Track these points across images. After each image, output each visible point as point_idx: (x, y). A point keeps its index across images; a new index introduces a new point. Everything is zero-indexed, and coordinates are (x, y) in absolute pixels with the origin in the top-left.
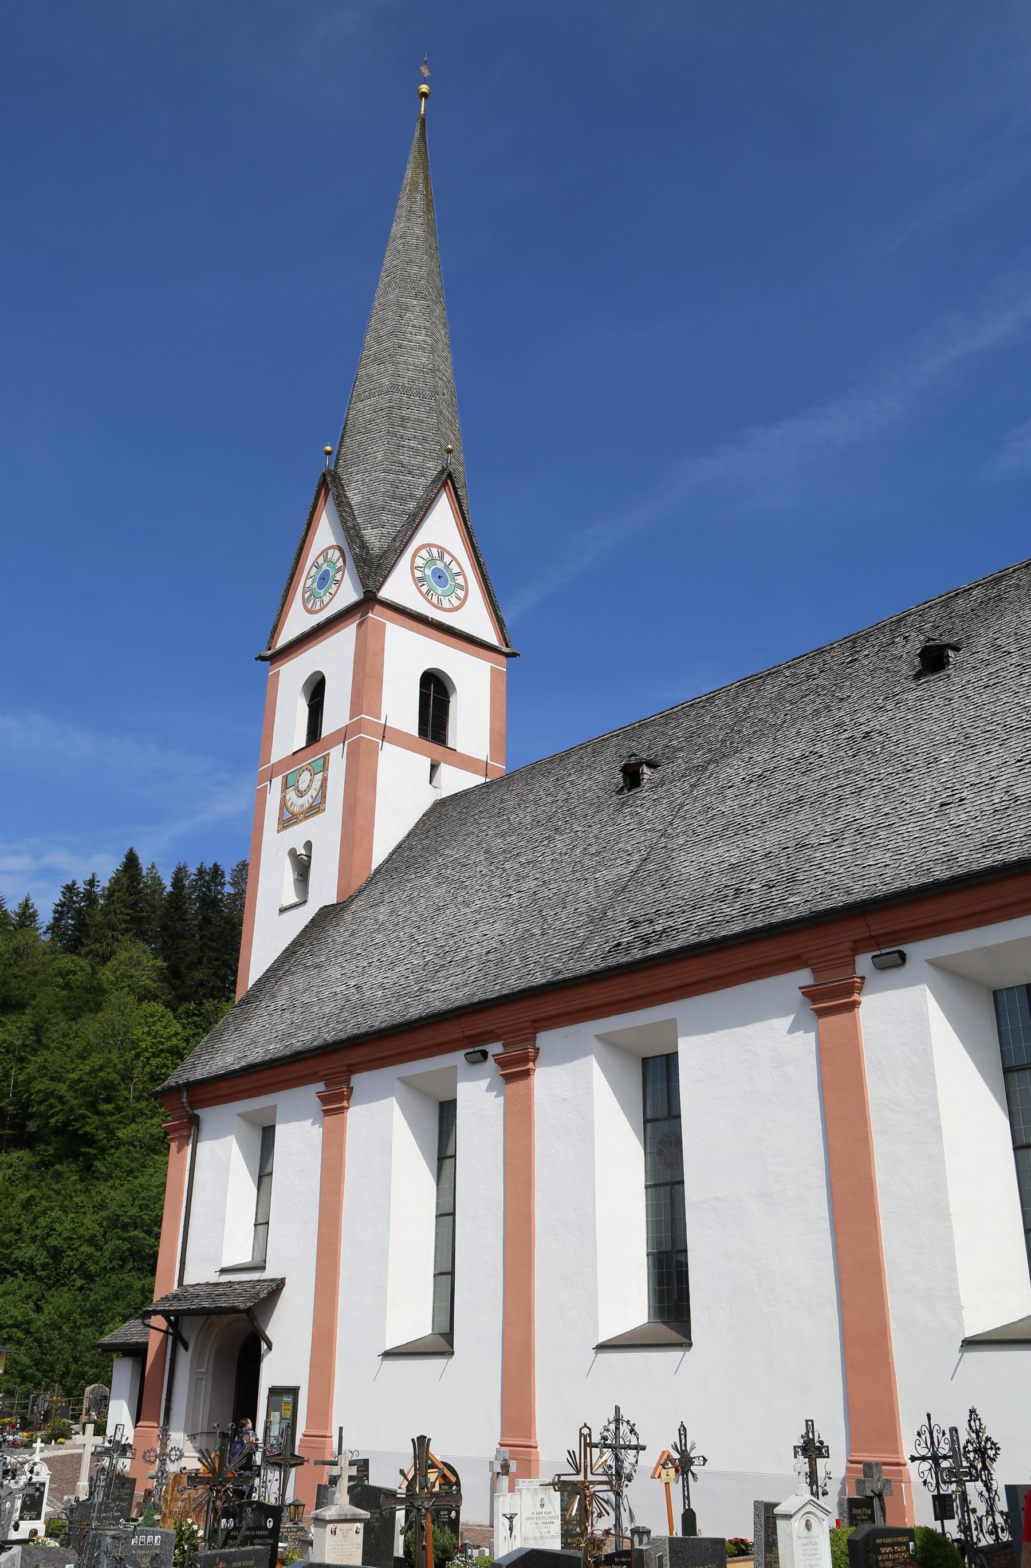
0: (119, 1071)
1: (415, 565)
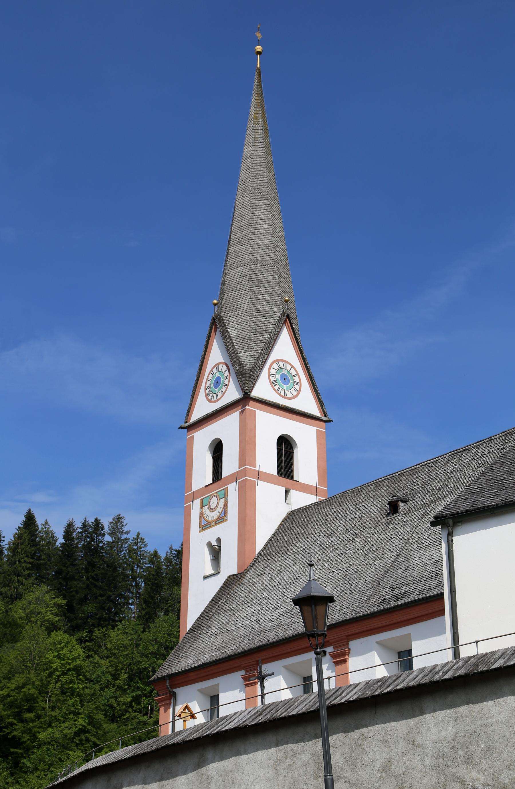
0: (36, 687)
1: (271, 374)
